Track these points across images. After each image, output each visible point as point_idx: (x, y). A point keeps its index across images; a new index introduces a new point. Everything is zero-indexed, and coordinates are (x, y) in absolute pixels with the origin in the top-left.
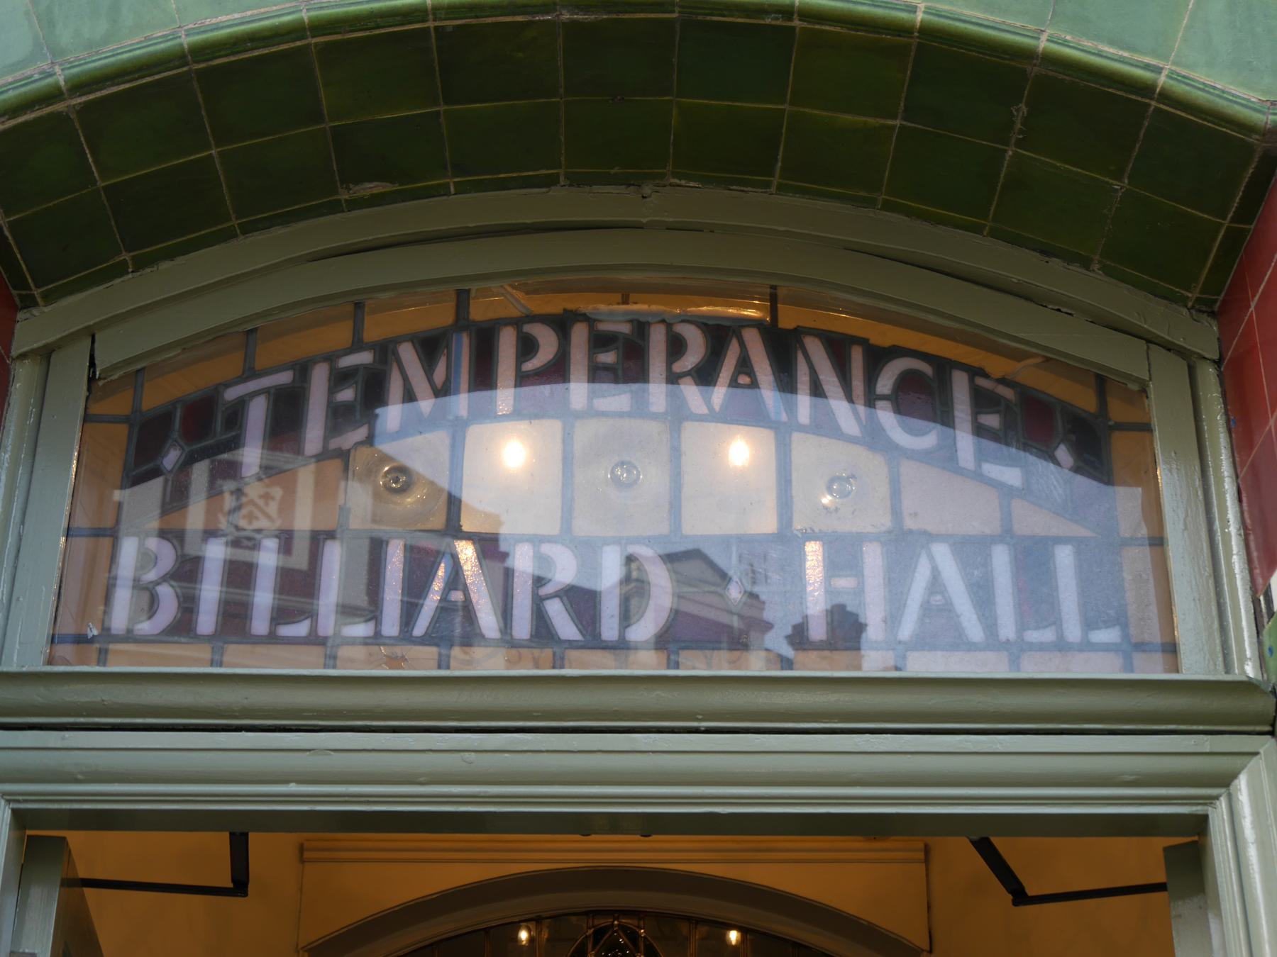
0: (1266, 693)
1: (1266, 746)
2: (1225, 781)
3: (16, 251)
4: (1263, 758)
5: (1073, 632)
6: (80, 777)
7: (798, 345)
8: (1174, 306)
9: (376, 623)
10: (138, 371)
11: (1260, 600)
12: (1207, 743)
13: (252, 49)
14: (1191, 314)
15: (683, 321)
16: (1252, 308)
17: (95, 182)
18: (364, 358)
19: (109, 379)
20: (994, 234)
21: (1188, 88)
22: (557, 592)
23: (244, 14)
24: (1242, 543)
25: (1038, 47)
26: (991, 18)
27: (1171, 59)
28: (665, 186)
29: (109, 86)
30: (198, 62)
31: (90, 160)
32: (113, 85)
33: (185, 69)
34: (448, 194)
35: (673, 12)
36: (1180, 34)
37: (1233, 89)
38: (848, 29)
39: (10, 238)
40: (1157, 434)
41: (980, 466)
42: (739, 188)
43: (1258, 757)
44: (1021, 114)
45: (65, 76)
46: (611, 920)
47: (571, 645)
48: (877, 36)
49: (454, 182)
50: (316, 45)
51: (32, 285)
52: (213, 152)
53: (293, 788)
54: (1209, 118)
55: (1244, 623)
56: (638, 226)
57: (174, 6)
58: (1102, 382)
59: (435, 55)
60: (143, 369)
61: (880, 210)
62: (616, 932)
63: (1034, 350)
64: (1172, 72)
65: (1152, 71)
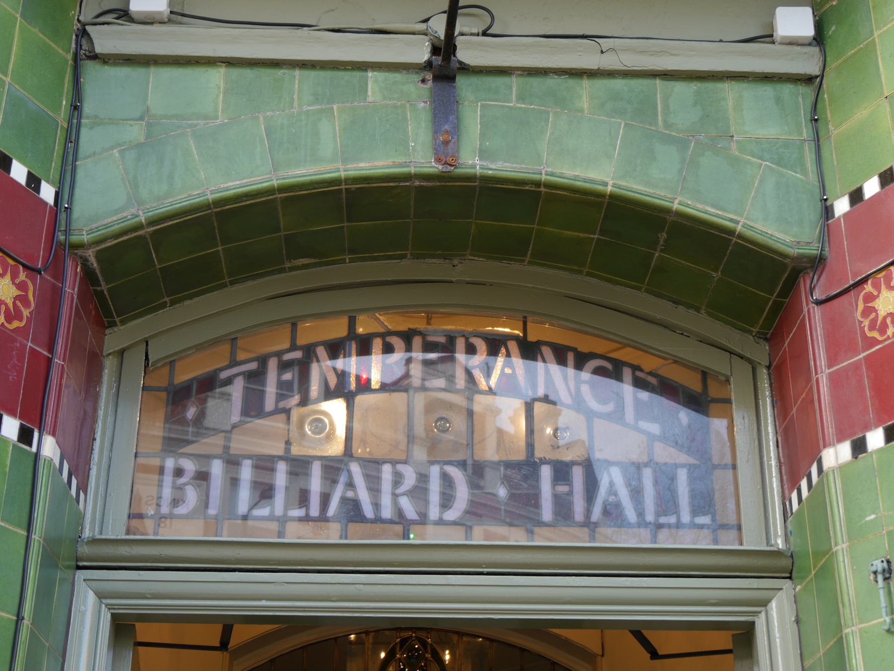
0: (787, 557)
1: (787, 585)
2: (765, 603)
3: (109, 301)
4: (785, 591)
5: (686, 518)
6: (149, 596)
7: (538, 351)
8: (745, 334)
9: (307, 509)
10: (171, 362)
11: (786, 504)
12: (756, 583)
13: (245, 201)
14: (754, 339)
15: (475, 336)
16: (786, 345)
17: (155, 265)
18: (298, 355)
19: (155, 366)
20: (647, 291)
21: (753, 233)
22: (405, 492)
23: (242, 182)
24: (778, 470)
25: (673, 207)
26: (648, 190)
27: (744, 216)
28: (465, 260)
29: (169, 221)
30: (216, 208)
31: (154, 256)
32: (171, 221)
33: (209, 211)
34: (345, 263)
35: (476, 182)
36: (750, 201)
37: (776, 234)
38: (570, 193)
39: (107, 295)
40: (734, 406)
41: (637, 423)
42: (507, 262)
43: (782, 591)
44: (663, 237)
45: (145, 217)
46: (411, 633)
47: (414, 522)
48: (586, 197)
49: (349, 258)
50: (281, 198)
51: (115, 316)
52: (220, 248)
53: (264, 603)
54: (764, 249)
55: (778, 516)
56: (452, 282)
57: (203, 176)
58: (704, 375)
59: (344, 201)
60: (174, 360)
61: (585, 275)
62: (414, 640)
63: (669, 357)
64: (745, 224)
65: (734, 223)
